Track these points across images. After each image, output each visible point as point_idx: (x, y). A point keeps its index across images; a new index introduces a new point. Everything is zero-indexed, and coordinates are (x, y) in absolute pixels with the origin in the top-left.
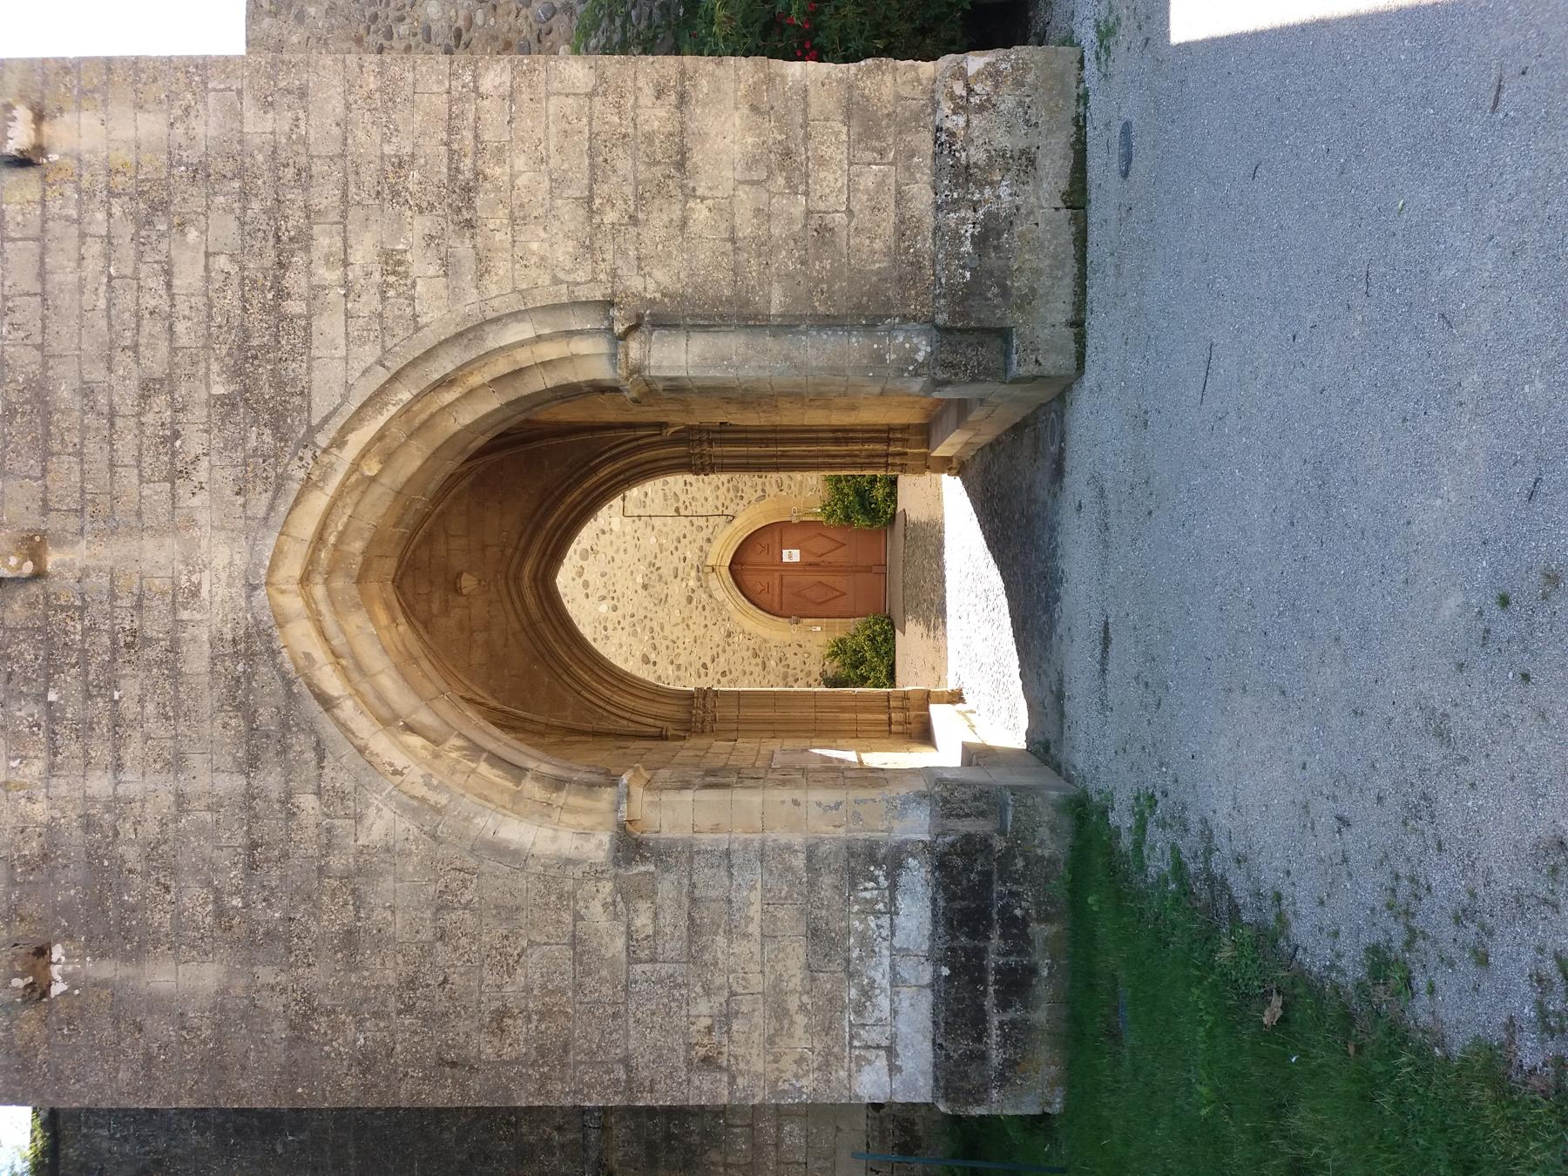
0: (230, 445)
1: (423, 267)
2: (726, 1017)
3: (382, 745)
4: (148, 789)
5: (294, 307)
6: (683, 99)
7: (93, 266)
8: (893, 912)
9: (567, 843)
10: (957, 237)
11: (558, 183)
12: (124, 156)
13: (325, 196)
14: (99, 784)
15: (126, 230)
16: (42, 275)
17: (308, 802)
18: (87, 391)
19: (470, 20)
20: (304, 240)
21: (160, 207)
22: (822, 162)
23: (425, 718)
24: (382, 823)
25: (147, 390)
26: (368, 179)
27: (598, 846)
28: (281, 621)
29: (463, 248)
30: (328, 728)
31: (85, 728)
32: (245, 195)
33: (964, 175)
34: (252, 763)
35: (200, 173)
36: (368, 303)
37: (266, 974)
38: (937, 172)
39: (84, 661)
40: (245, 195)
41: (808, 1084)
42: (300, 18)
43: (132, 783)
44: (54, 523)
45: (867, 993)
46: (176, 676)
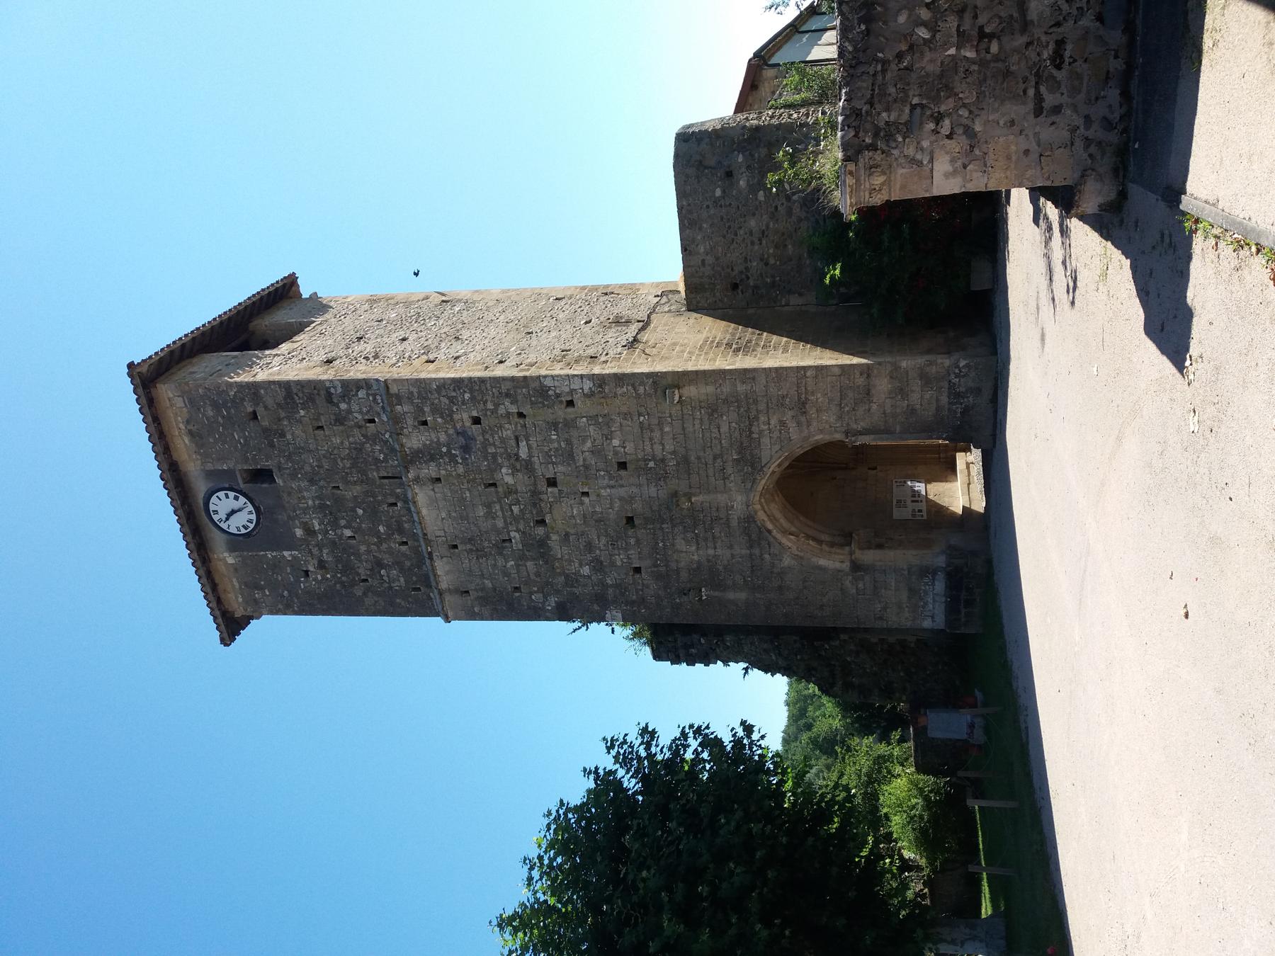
0: (739, 471)
1: (792, 425)
2: (885, 609)
3: (784, 541)
4: (723, 553)
5: (755, 436)
6: (869, 376)
7: (697, 426)
8: (933, 584)
9: (838, 565)
10: (955, 412)
11: (831, 400)
12: (703, 397)
13: (762, 407)
14: (711, 552)
15: (706, 418)
16: (684, 429)
17: (767, 556)
18: (699, 458)
19: (767, 226)
20: (757, 418)
21: (715, 411)
22: (913, 391)
23: (793, 529)
24: (787, 561)
25: (715, 458)
26: (774, 402)
27: (846, 566)
28: (756, 512)
29: (803, 419)
30: (772, 540)
31: (706, 539)
32: (739, 407)
33: (958, 395)
34: (751, 547)
35: (726, 401)
36: (776, 434)
37: (758, 595)
38: (950, 393)
39: (704, 523)
40: (739, 407)
41: (909, 624)
42: (700, 229)
43: (719, 552)
44: (693, 491)
45: (926, 604)
46: (729, 527)
